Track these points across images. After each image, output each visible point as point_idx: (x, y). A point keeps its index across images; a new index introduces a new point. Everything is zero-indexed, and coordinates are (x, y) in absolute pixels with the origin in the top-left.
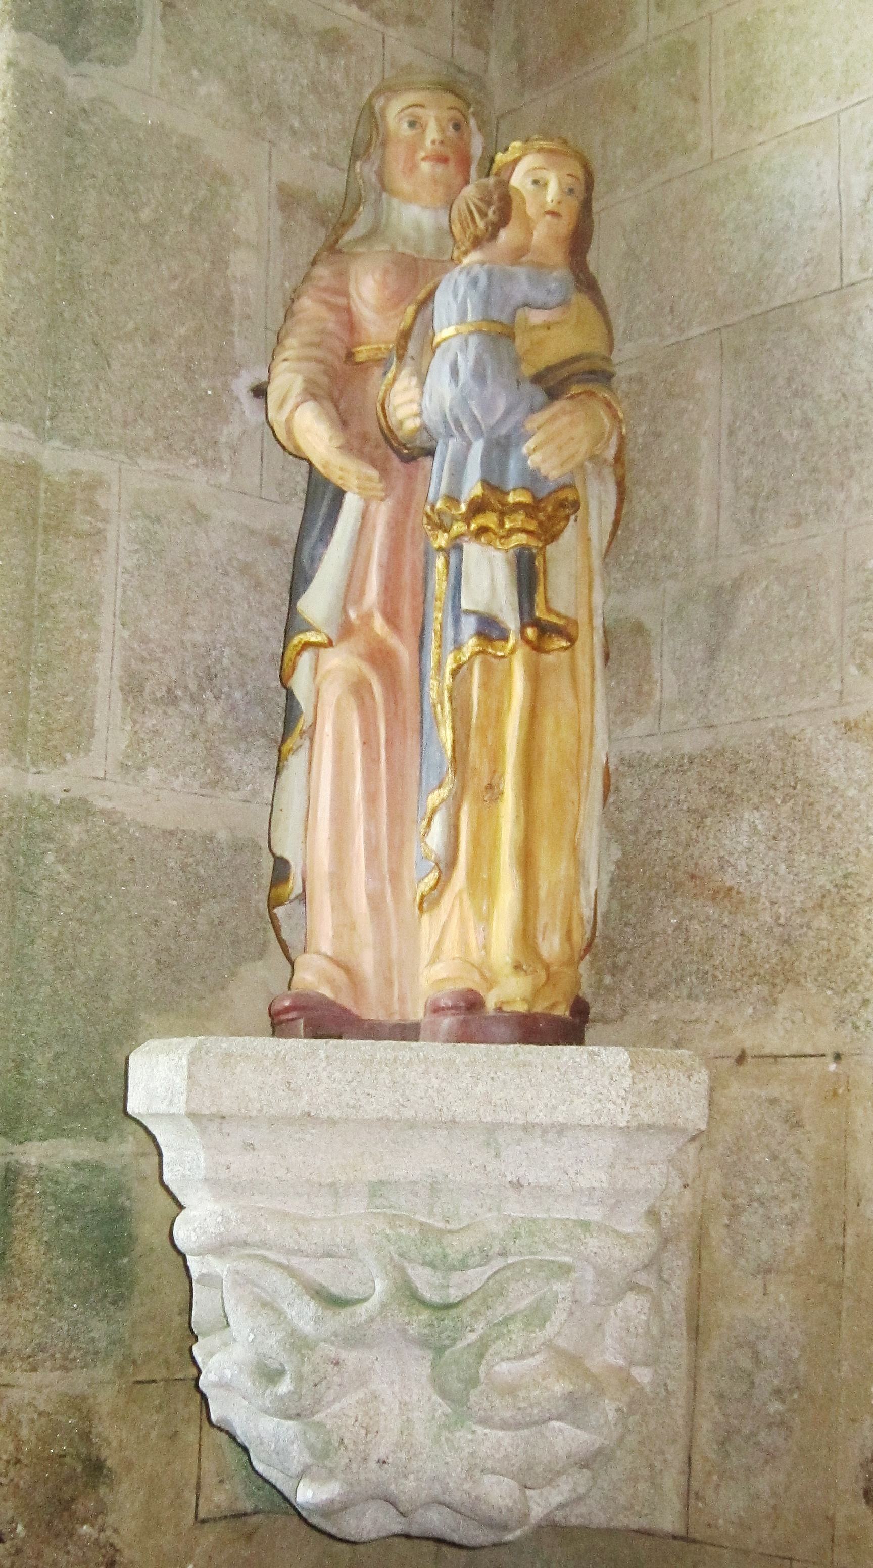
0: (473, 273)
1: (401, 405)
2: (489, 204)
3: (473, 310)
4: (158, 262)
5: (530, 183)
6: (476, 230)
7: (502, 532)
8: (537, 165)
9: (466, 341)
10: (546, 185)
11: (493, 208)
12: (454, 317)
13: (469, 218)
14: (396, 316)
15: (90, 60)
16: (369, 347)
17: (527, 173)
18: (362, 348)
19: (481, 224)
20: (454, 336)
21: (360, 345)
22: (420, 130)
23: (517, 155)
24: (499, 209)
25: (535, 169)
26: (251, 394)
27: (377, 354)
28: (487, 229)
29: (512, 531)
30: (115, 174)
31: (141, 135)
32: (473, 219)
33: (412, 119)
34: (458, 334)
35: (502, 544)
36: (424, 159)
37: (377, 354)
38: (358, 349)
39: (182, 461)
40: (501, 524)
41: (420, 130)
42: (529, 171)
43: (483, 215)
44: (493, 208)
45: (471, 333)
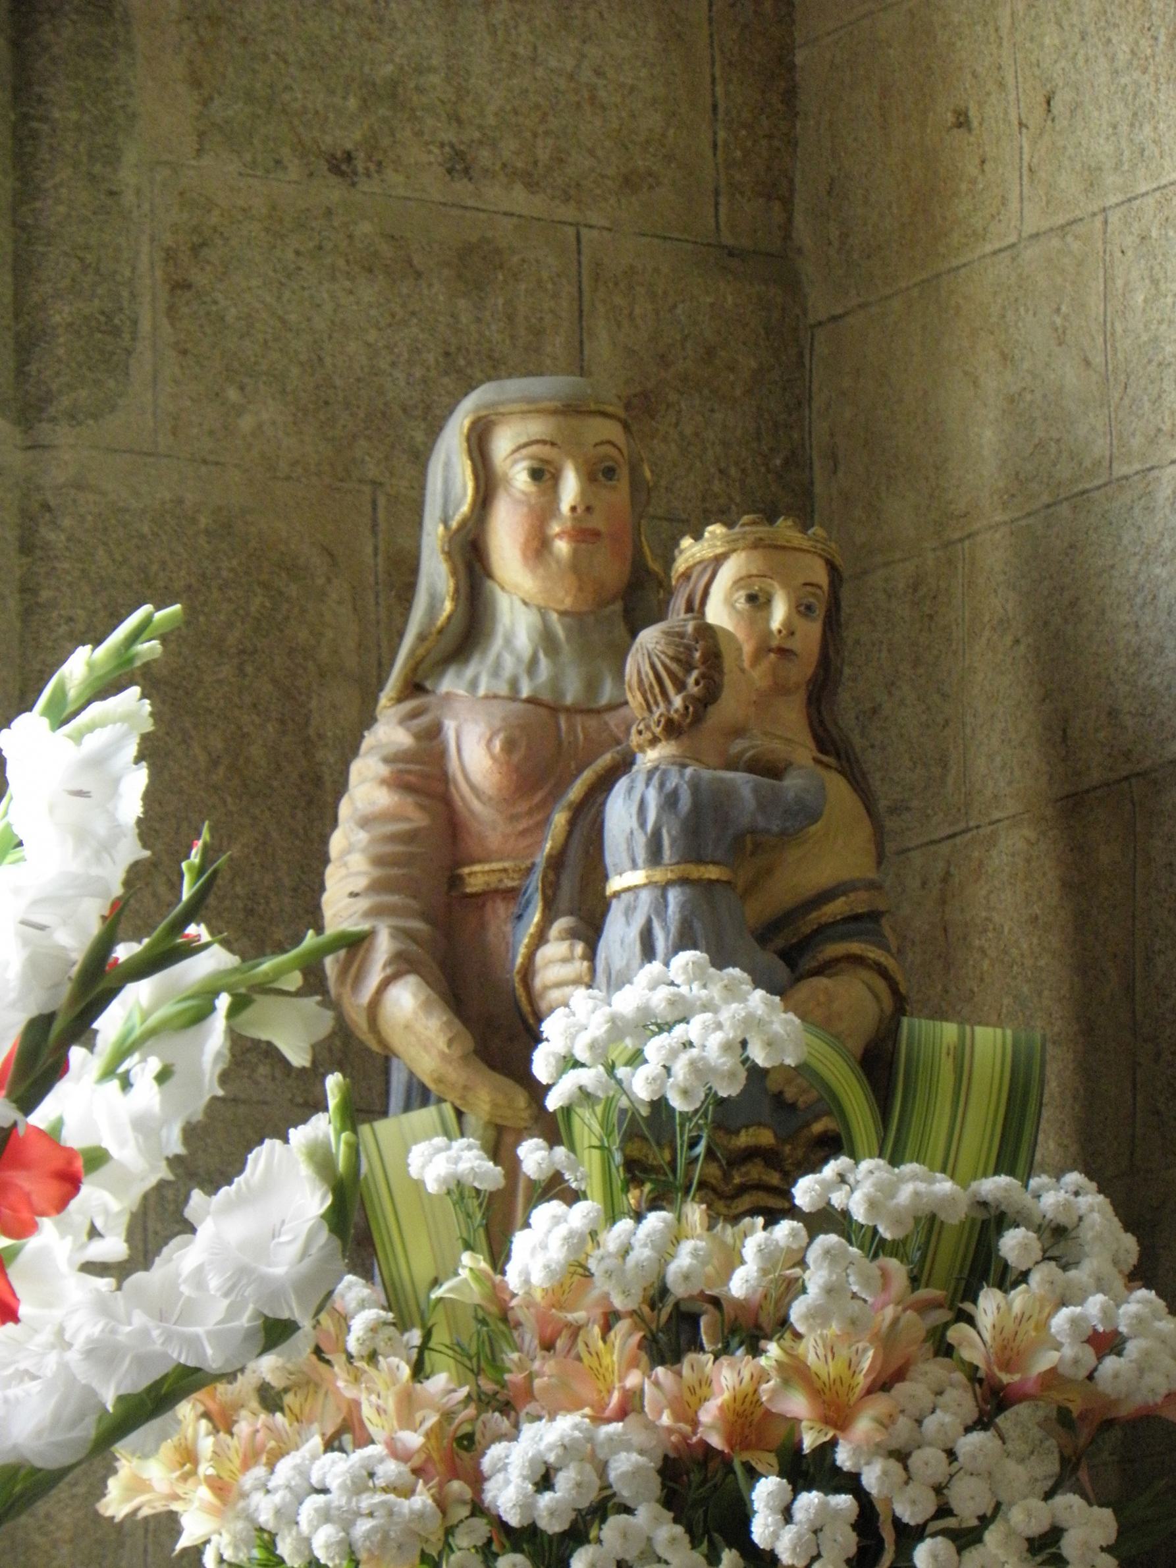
0: (670, 785)
1: (551, 962)
2: (688, 667)
3: (672, 846)
4: (185, 740)
5: (742, 600)
6: (668, 711)
7: (728, 1189)
8: (755, 572)
9: (664, 897)
10: (769, 602)
11: (695, 674)
12: (641, 855)
13: (657, 690)
14: (530, 812)
15: (53, 420)
16: (487, 867)
17: (738, 583)
18: (477, 868)
19: (678, 701)
20: (645, 885)
21: (473, 862)
22: (550, 483)
23: (720, 550)
24: (703, 676)
25: (750, 576)
26: (1025, 1545)
27: (501, 881)
28: (686, 708)
29: (742, 1190)
30: (105, 607)
31: (145, 529)
32: (664, 692)
33: (536, 465)
34: (649, 884)
35: (728, 1207)
36: (559, 535)
37: (501, 881)
38: (466, 870)
39: (246, 1072)
40: (727, 1177)
41: (550, 483)
42: (741, 579)
43: (680, 686)
44: (695, 674)
45: (670, 883)
